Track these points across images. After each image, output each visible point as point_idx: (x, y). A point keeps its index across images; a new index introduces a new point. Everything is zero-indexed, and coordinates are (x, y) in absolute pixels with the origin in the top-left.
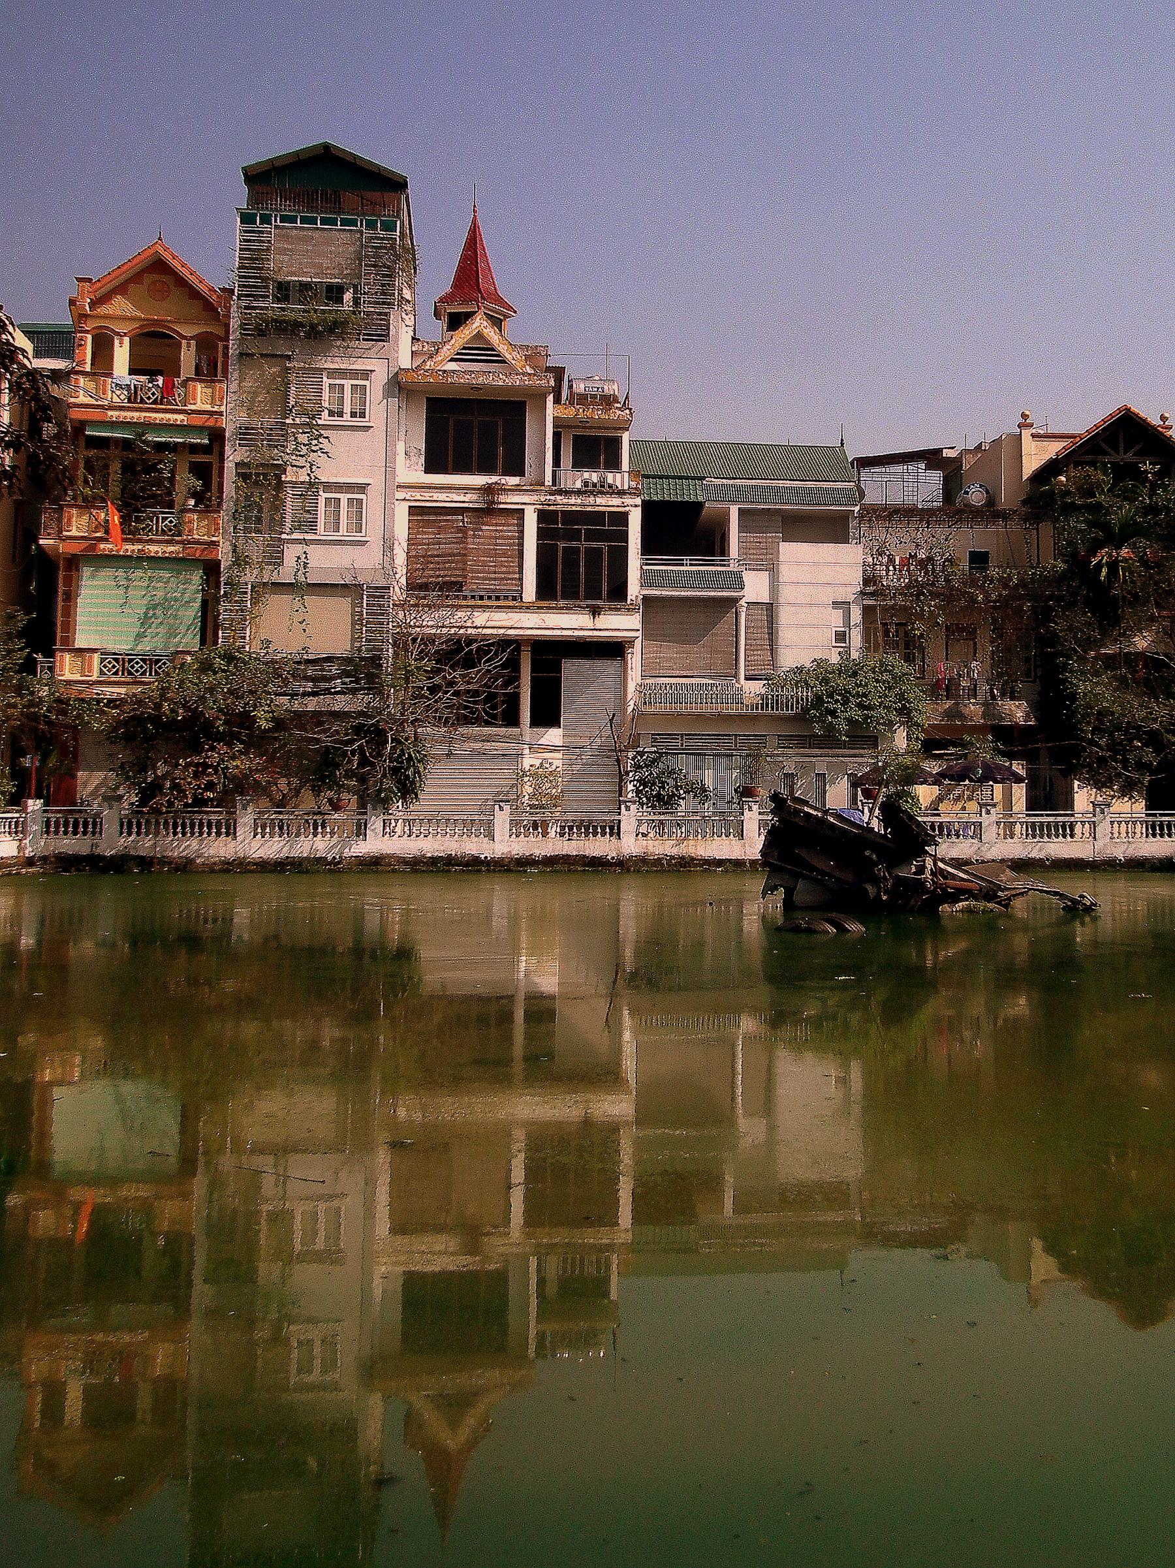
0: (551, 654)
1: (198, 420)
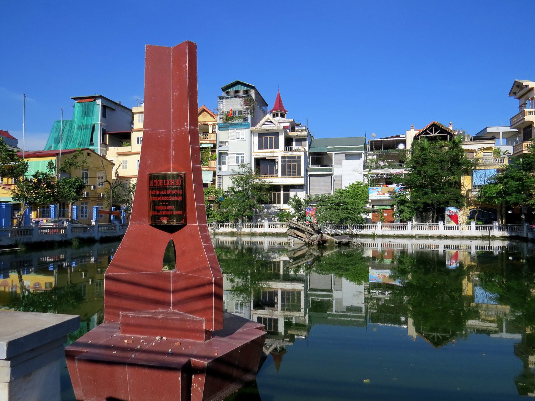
0: (287, 188)
1: (212, 142)
